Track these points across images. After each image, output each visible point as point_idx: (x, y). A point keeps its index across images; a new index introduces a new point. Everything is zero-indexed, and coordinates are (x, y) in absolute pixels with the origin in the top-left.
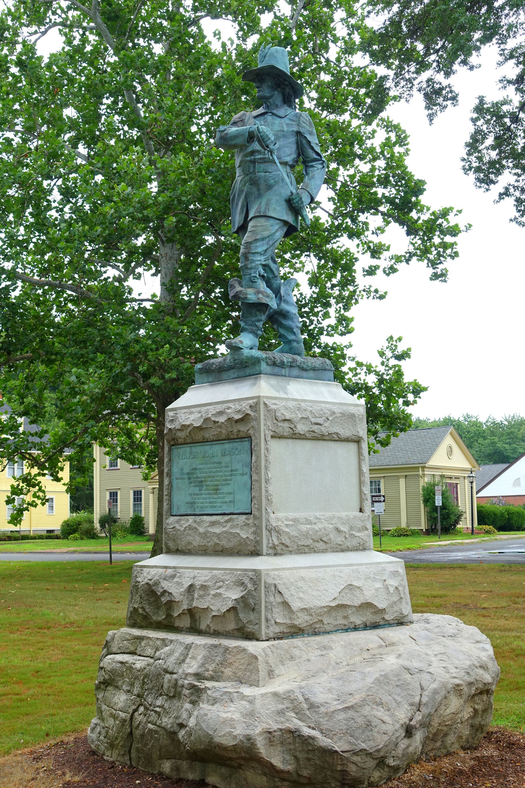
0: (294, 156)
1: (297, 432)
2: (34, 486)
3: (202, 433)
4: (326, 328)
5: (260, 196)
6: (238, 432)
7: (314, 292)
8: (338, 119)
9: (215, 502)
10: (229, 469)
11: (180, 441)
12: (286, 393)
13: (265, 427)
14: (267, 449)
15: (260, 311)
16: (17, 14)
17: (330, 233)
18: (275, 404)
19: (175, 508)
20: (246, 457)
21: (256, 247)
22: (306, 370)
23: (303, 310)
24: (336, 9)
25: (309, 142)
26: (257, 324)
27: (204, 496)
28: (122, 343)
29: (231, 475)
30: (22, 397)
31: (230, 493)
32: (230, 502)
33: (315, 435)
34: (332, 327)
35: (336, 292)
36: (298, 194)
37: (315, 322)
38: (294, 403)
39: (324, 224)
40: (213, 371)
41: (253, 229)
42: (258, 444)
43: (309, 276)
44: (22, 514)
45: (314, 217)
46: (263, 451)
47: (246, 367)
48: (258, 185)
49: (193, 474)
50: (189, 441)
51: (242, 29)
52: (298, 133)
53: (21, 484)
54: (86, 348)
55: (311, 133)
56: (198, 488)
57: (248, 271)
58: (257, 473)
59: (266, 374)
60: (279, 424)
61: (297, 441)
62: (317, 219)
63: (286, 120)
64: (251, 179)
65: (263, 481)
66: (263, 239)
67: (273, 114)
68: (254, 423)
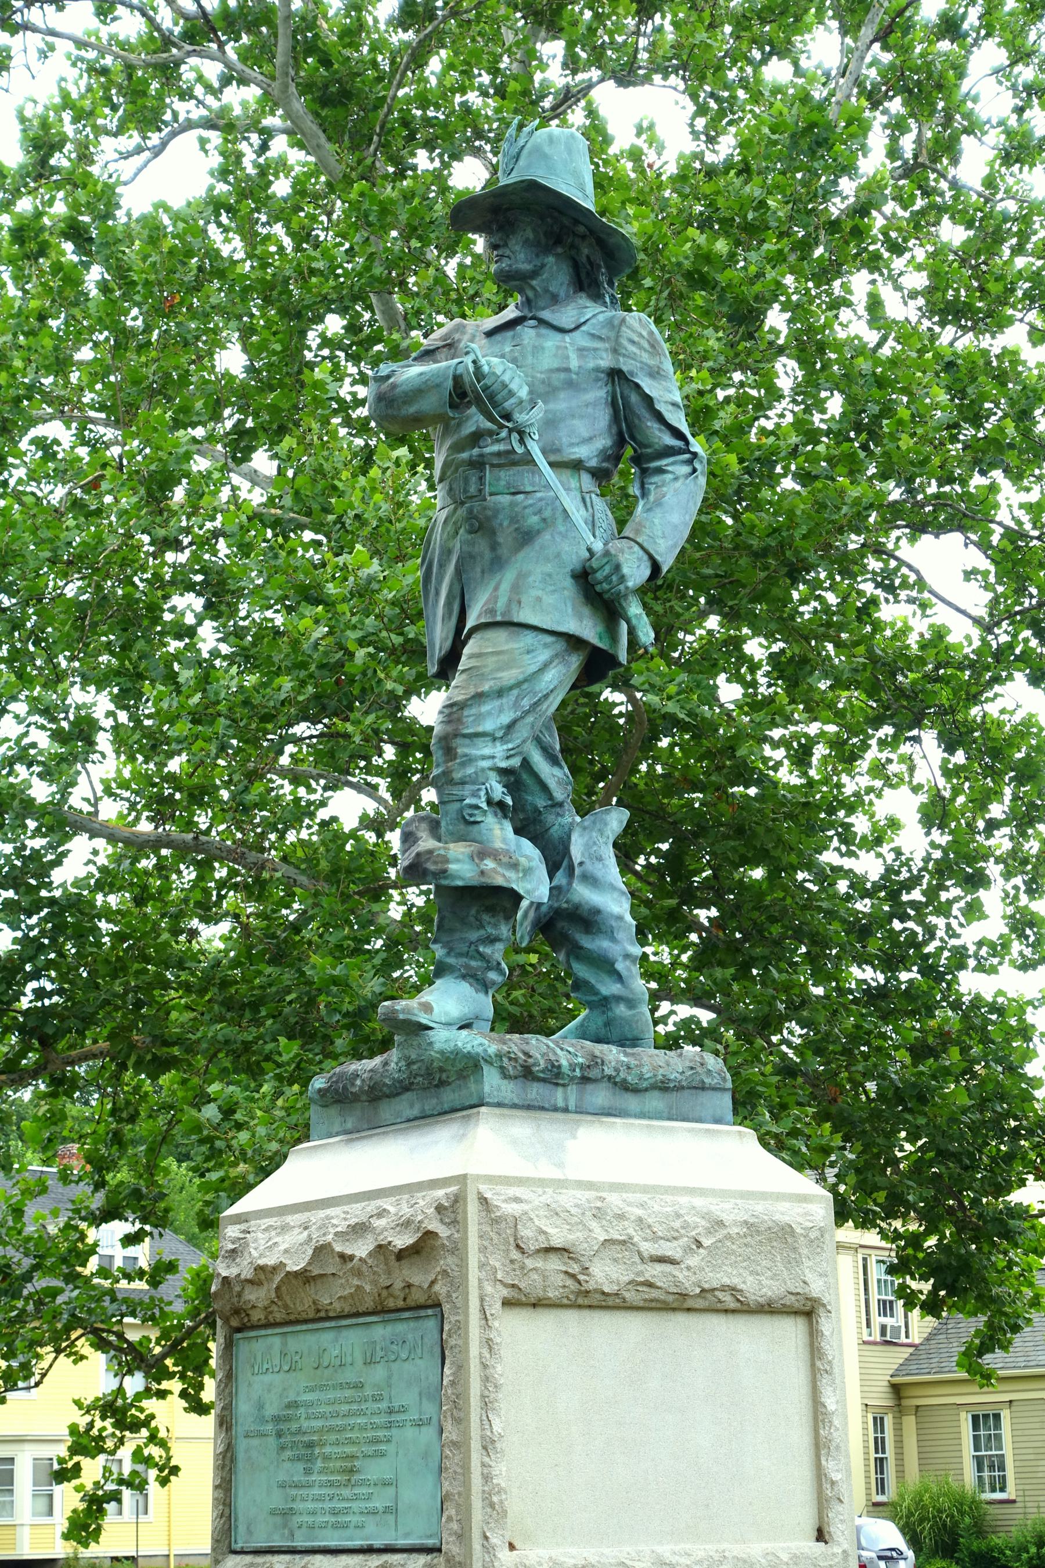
0: (604, 442)
1: (591, 1285)
2: (135, 1426)
3: (311, 1289)
4: (972, 949)
5: (497, 564)
6: (402, 1289)
7: (933, 845)
8: (984, 345)
9: (346, 1511)
10: (383, 1405)
11: (257, 1316)
12: (560, 1165)
13: (480, 1274)
14: (489, 1344)
15: (491, 910)
16: (87, 104)
17: (977, 674)
18: (517, 1200)
19: (242, 1529)
20: (424, 1366)
21: (480, 718)
22: (636, 1090)
23: (905, 898)
24: (976, 43)
25: (648, 400)
26: (486, 950)
27: (316, 1491)
28: (346, 1007)
29: (389, 1425)
30: (100, 1166)
31: (386, 1484)
32: (387, 1510)
33: (654, 1294)
34: (992, 945)
35: (1001, 841)
36: (607, 553)
37: (940, 933)
38: (584, 1196)
39: (960, 645)
40: (356, 1098)
41: (473, 663)
42: (461, 1327)
43: (923, 798)
44: (101, 1511)
45: (931, 626)
46: (474, 1349)
47: (442, 1083)
48: (493, 533)
49: (288, 1419)
50: (279, 1316)
51: (702, 110)
52: (615, 375)
53: (98, 1424)
54: (258, 1022)
55: (655, 374)
56: (300, 1466)
57: (456, 791)
58: (458, 1421)
59: (499, 1105)
60: (530, 1263)
61: (598, 1316)
62: (939, 634)
63: (580, 338)
64: (471, 516)
65: (475, 1445)
66: (500, 693)
67: (542, 322)
68: (448, 1262)
